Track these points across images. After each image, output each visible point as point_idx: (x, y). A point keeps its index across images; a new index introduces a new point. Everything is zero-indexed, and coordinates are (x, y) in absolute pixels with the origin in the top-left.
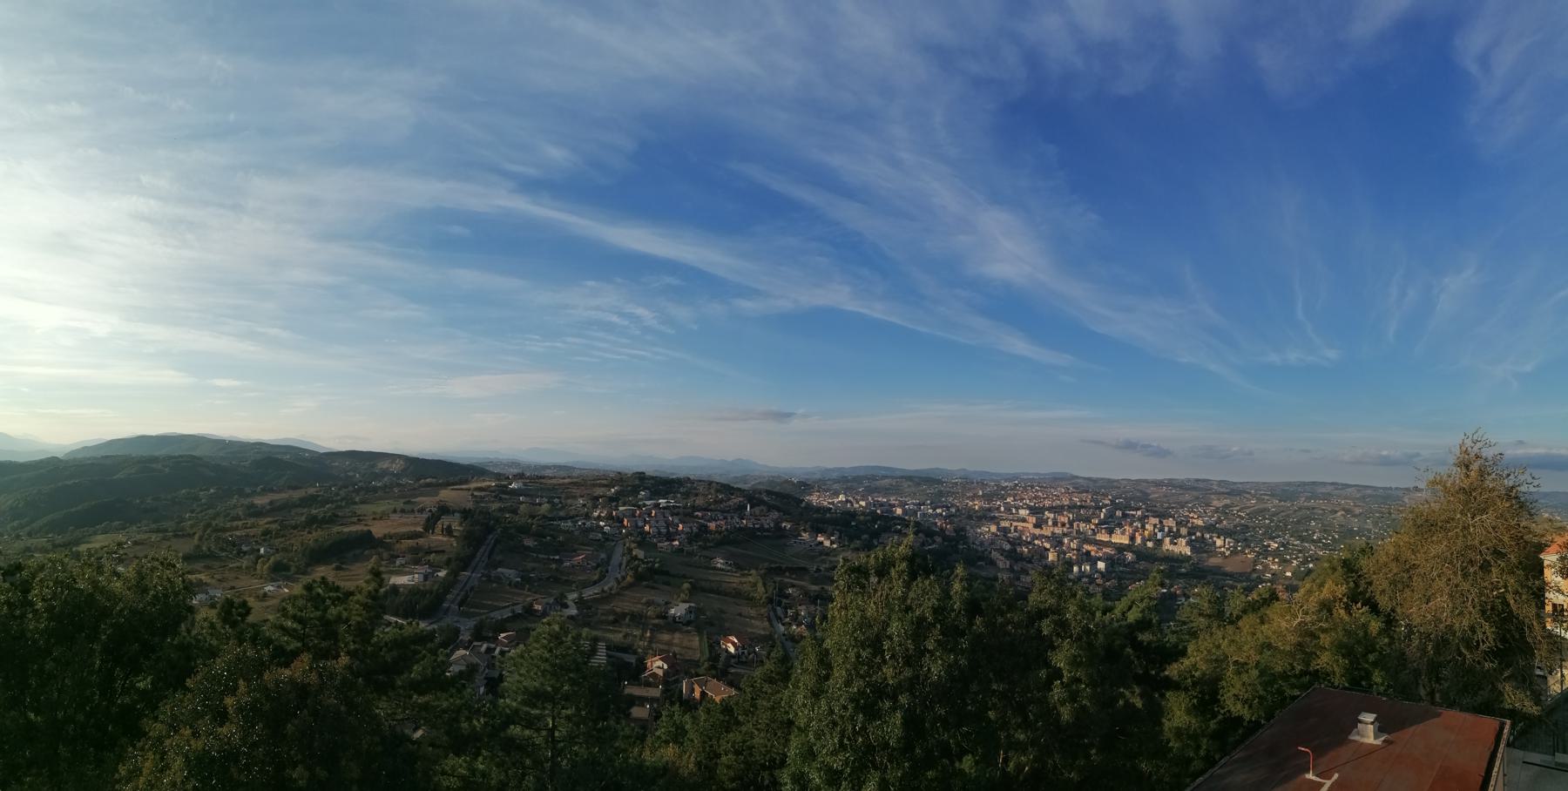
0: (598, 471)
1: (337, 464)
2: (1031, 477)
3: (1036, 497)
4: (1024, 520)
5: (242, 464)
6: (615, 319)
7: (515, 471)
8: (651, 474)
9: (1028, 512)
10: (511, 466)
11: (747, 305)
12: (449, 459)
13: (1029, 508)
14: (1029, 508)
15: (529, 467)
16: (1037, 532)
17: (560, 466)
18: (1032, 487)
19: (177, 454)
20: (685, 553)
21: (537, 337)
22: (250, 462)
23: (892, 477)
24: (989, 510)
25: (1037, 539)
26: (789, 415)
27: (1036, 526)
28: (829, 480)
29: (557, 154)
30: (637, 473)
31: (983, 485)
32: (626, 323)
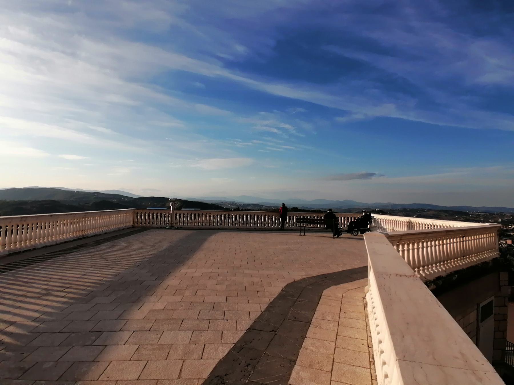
0: (273, 207)
1: (143, 204)
5: (86, 204)
6: (275, 130)
7: (235, 207)
8: (300, 208)
10: (232, 205)
11: (340, 119)
15: (240, 205)
19: (40, 200)
21: (240, 140)
22: (91, 203)
23: (435, 211)
24: (506, 230)
26: (372, 175)
28: (396, 210)
29: (240, 49)
30: (294, 208)
31: (501, 216)
32: (281, 133)
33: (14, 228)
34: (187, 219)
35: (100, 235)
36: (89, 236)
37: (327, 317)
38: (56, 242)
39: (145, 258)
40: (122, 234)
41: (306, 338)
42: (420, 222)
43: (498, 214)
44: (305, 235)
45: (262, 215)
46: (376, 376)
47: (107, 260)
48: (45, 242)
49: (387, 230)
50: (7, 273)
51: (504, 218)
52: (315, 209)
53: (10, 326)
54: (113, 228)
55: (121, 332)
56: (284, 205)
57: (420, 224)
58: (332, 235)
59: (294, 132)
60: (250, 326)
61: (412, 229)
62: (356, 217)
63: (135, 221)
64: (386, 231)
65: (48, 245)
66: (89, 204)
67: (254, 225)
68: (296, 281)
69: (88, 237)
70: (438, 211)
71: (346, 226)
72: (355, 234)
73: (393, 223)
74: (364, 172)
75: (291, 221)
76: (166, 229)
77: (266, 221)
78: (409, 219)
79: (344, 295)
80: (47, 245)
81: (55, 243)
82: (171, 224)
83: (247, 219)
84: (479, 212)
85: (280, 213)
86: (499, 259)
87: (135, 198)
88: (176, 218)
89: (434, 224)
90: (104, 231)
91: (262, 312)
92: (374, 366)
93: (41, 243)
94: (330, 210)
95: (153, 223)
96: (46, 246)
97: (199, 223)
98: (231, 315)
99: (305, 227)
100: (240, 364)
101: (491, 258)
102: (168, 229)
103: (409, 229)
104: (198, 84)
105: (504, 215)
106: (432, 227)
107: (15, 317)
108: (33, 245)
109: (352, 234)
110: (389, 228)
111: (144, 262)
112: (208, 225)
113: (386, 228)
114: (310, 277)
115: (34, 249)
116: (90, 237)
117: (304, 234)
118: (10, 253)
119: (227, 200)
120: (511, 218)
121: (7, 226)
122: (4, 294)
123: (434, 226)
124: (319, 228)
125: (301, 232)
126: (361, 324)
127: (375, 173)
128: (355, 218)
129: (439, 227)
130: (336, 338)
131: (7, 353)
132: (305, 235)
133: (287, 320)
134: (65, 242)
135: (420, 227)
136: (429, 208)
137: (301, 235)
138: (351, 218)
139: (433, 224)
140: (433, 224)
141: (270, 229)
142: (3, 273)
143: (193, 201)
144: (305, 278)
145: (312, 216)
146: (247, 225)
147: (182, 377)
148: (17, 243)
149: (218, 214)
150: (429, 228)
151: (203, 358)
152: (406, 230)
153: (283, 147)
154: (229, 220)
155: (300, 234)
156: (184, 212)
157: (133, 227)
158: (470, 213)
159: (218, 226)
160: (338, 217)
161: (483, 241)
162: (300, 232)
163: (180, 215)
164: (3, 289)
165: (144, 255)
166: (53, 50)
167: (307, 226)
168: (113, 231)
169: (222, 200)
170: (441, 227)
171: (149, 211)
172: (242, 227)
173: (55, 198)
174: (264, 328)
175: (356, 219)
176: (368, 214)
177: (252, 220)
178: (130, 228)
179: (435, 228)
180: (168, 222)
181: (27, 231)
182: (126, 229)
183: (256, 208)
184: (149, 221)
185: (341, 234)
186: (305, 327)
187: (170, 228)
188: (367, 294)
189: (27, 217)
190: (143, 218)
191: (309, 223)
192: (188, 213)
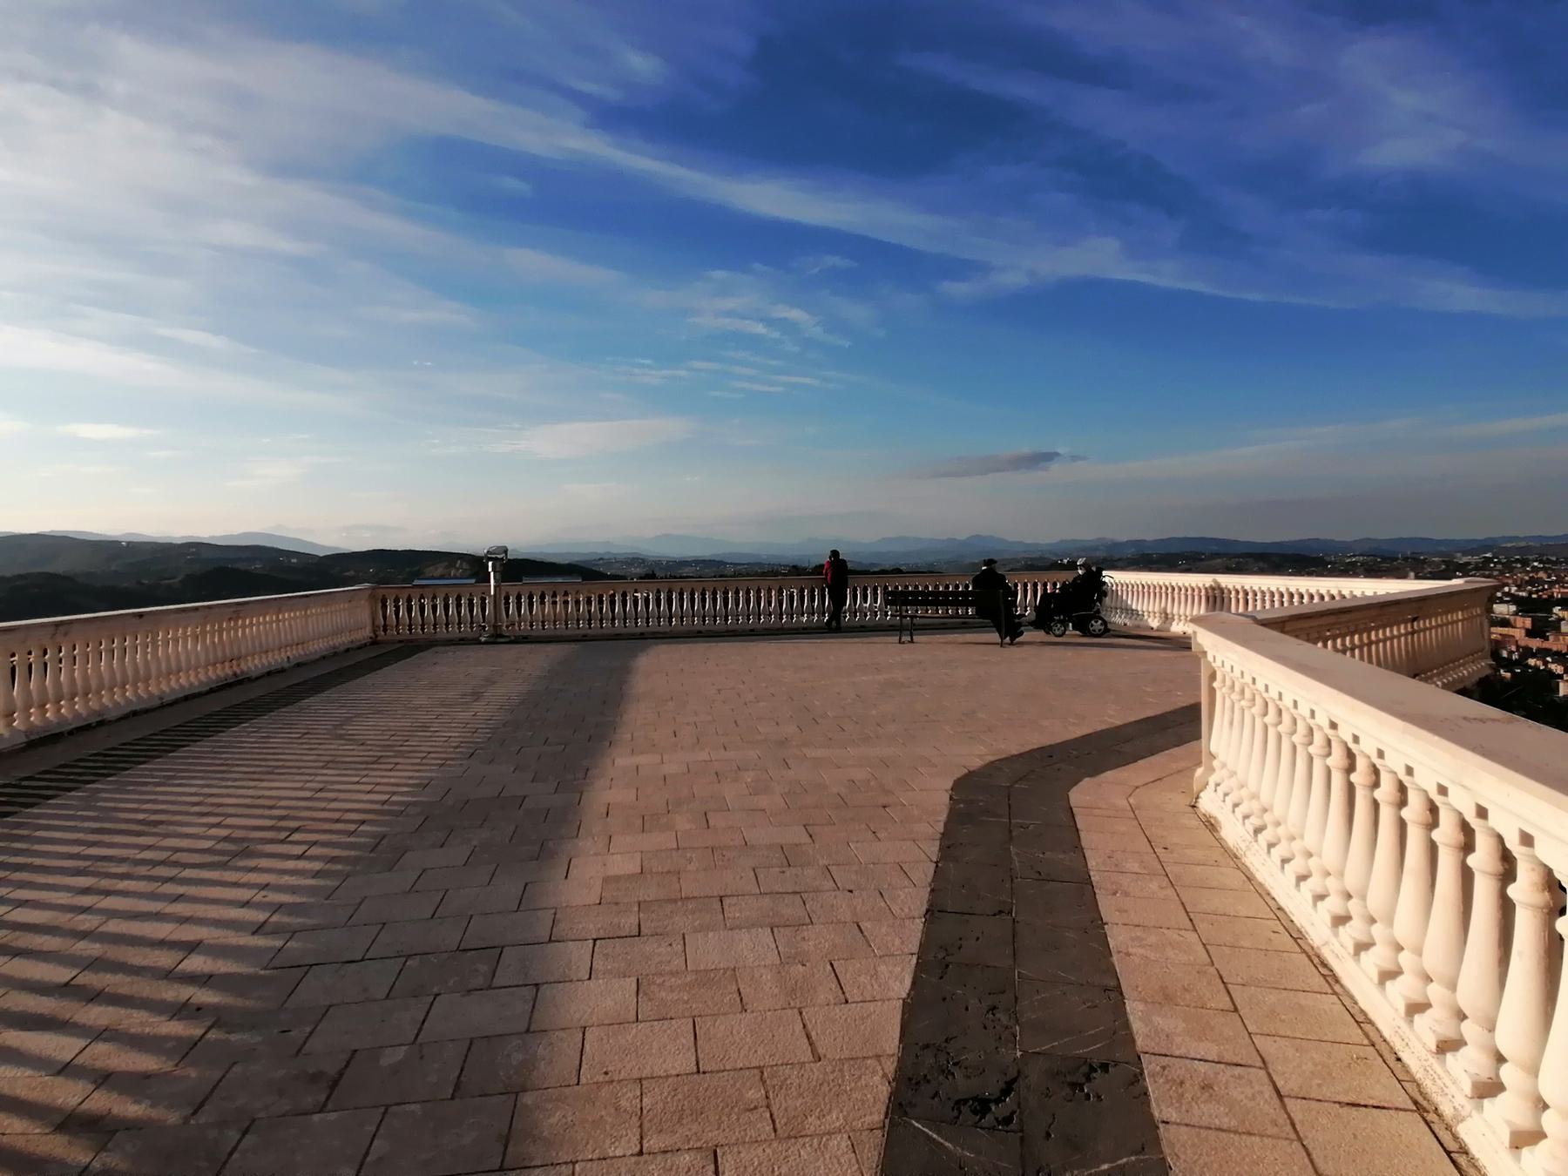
0: (759, 564)
1: (352, 573)
2: (1523, 544)
3: (1532, 582)
4: (1505, 623)
5: (163, 582)
6: (760, 329)
9: (1513, 608)
10: (632, 564)
11: (958, 289)
12: (538, 558)
13: (1515, 600)
14: (1515, 600)
15: (658, 563)
16: (1535, 644)
17: (704, 561)
18: (1525, 563)
20: (66, 735)
21: (648, 362)
22: (180, 578)
25: (1533, 655)
26: (1049, 457)
27: (1530, 633)
28: (1119, 560)
29: (642, 65)
32: (776, 335)
33: (35, 657)
34: (519, 611)
35: (282, 671)
36: (254, 675)
37: (1128, 865)
38: (161, 698)
39: (476, 732)
40: (351, 666)
41: (1106, 924)
42: (1247, 587)
43: (1406, 559)
44: (912, 641)
45: (659, 591)
46: (1362, 1011)
47: (362, 744)
48: (128, 701)
49: (1143, 615)
50: (39, 808)
51: (1424, 568)
52: (883, 568)
53: (189, 954)
54: (318, 647)
55: (552, 944)
56: (835, 553)
57: (1272, 594)
58: (995, 637)
60: (925, 902)
61: (1221, 609)
62: (1055, 582)
63: (376, 623)
64: (1141, 620)
65: (138, 708)
66: (172, 581)
67: (682, 621)
68: (974, 771)
69: (250, 680)
70: (1239, 556)
71: (1028, 609)
72: (1057, 632)
73: (1152, 594)
74: (1026, 450)
75: (867, 603)
76: (480, 643)
77: (770, 604)
78: (1215, 581)
79: (1131, 800)
80: (134, 709)
81: (157, 703)
82: (495, 627)
83: (748, 601)
84: (1354, 556)
85: (826, 579)
86: (1492, 678)
87: (321, 555)
88: (507, 610)
89: (1293, 590)
90: (291, 657)
91: (937, 863)
92: (1342, 986)
93: (117, 704)
94: (990, 562)
95: (435, 628)
96: (135, 713)
97: (578, 620)
98: (854, 877)
99: (912, 617)
100: (967, 1009)
101: (1475, 678)
102: (486, 643)
103: (1214, 609)
104: (512, 184)
105: (1424, 561)
106: (1296, 599)
107: (184, 926)
108: (95, 711)
109: (1048, 631)
110: (1150, 610)
111: (482, 742)
112: (549, 628)
113: (1139, 609)
114: (1006, 759)
115: (101, 723)
116: (258, 678)
117: (910, 640)
118: (32, 737)
119: (614, 551)
120: (1443, 567)
121: (13, 655)
122: (99, 863)
123: (1302, 596)
124: (951, 617)
125: (905, 632)
126: (1234, 879)
127: (1059, 450)
128: (1055, 584)
129: (1316, 600)
130: (1191, 920)
131: (233, 1037)
132: (912, 641)
133: (1019, 880)
134: (186, 698)
135: (1231, 599)
136: (1215, 548)
137: (904, 643)
138: (1045, 585)
139: (1287, 589)
140: (1287, 589)
141: (797, 629)
142: (50, 799)
144: (992, 762)
145: (942, 585)
146: (671, 622)
147: (825, 1056)
148: (15, 715)
149: (624, 590)
150: (1286, 604)
151: (532, 1030)
152: (1203, 611)
153: (784, 379)
154: (613, 610)
155: (900, 639)
157: (374, 642)
158: (1327, 559)
159: (637, 629)
160: (1016, 585)
161: (1428, 637)
162: (898, 633)
163: (519, 598)
164: (82, 853)
165: (468, 724)
166: (22, 76)
167: (927, 615)
168: (317, 657)
169: (601, 550)
170: (1322, 597)
171: (420, 591)
172: (713, 628)
173: (58, 568)
174: (971, 907)
175: (1058, 587)
176: (1094, 569)
177: (740, 605)
178: (365, 645)
179: (1304, 601)
180: (484, 622)
181: (60, 666)
182: (352, 649)
183: (707, 570)
184: (447, 619)
185: (1021, 634)
186: (1084, 894)
187: (492, 640)
188: (1202, 795)
189: (71, 622)
190: (406, 614)
191: (952, 604)
192: (681, 589)
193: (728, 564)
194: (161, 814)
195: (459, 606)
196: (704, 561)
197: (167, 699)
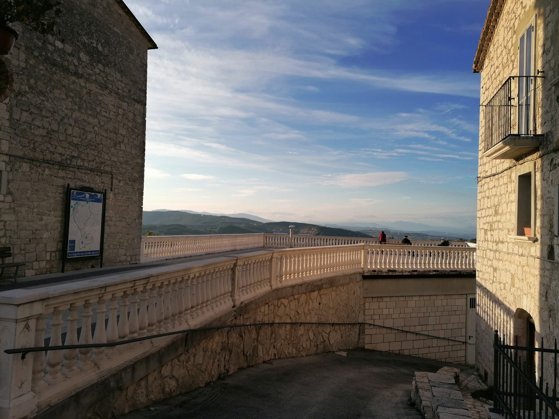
6: (426, 135)
12: (345, 228)
17: (417, 234)
19: (168, 224)
21: (380, 150)
32: (434, 138)
35: (243, 250)
59: (454, 136)
69: (237, 250)
81: (184, 256)
82: (291, 245)
87: (264, 223)
119: (377, 227)
143: (333, 227)
156: (300, 236)
169: (371, 226)
171: (274, 236)
193: (429, 236)
194: (534, 204)
195: (286, 240)
196: (418, 234)
197: (174, 257)
